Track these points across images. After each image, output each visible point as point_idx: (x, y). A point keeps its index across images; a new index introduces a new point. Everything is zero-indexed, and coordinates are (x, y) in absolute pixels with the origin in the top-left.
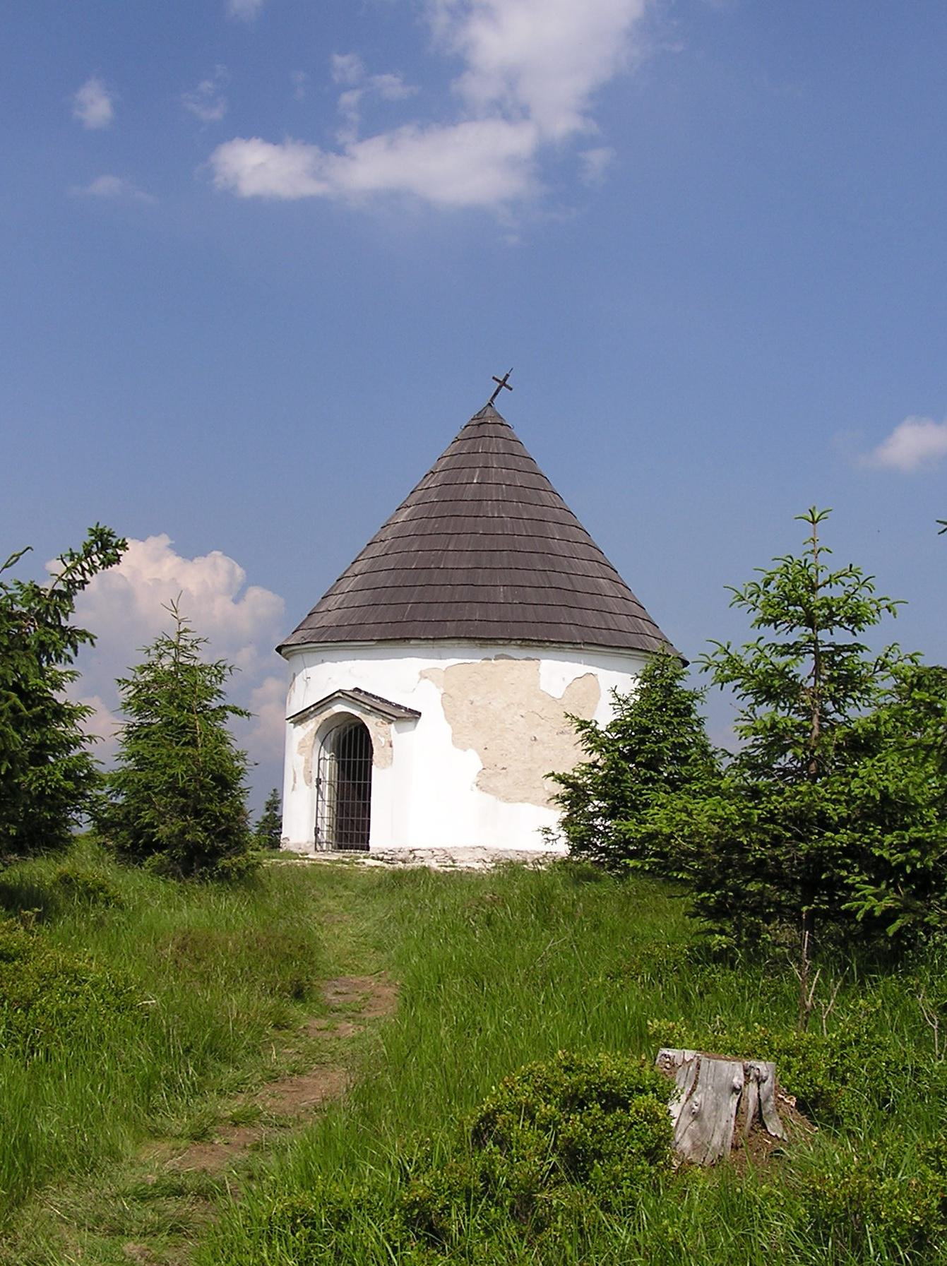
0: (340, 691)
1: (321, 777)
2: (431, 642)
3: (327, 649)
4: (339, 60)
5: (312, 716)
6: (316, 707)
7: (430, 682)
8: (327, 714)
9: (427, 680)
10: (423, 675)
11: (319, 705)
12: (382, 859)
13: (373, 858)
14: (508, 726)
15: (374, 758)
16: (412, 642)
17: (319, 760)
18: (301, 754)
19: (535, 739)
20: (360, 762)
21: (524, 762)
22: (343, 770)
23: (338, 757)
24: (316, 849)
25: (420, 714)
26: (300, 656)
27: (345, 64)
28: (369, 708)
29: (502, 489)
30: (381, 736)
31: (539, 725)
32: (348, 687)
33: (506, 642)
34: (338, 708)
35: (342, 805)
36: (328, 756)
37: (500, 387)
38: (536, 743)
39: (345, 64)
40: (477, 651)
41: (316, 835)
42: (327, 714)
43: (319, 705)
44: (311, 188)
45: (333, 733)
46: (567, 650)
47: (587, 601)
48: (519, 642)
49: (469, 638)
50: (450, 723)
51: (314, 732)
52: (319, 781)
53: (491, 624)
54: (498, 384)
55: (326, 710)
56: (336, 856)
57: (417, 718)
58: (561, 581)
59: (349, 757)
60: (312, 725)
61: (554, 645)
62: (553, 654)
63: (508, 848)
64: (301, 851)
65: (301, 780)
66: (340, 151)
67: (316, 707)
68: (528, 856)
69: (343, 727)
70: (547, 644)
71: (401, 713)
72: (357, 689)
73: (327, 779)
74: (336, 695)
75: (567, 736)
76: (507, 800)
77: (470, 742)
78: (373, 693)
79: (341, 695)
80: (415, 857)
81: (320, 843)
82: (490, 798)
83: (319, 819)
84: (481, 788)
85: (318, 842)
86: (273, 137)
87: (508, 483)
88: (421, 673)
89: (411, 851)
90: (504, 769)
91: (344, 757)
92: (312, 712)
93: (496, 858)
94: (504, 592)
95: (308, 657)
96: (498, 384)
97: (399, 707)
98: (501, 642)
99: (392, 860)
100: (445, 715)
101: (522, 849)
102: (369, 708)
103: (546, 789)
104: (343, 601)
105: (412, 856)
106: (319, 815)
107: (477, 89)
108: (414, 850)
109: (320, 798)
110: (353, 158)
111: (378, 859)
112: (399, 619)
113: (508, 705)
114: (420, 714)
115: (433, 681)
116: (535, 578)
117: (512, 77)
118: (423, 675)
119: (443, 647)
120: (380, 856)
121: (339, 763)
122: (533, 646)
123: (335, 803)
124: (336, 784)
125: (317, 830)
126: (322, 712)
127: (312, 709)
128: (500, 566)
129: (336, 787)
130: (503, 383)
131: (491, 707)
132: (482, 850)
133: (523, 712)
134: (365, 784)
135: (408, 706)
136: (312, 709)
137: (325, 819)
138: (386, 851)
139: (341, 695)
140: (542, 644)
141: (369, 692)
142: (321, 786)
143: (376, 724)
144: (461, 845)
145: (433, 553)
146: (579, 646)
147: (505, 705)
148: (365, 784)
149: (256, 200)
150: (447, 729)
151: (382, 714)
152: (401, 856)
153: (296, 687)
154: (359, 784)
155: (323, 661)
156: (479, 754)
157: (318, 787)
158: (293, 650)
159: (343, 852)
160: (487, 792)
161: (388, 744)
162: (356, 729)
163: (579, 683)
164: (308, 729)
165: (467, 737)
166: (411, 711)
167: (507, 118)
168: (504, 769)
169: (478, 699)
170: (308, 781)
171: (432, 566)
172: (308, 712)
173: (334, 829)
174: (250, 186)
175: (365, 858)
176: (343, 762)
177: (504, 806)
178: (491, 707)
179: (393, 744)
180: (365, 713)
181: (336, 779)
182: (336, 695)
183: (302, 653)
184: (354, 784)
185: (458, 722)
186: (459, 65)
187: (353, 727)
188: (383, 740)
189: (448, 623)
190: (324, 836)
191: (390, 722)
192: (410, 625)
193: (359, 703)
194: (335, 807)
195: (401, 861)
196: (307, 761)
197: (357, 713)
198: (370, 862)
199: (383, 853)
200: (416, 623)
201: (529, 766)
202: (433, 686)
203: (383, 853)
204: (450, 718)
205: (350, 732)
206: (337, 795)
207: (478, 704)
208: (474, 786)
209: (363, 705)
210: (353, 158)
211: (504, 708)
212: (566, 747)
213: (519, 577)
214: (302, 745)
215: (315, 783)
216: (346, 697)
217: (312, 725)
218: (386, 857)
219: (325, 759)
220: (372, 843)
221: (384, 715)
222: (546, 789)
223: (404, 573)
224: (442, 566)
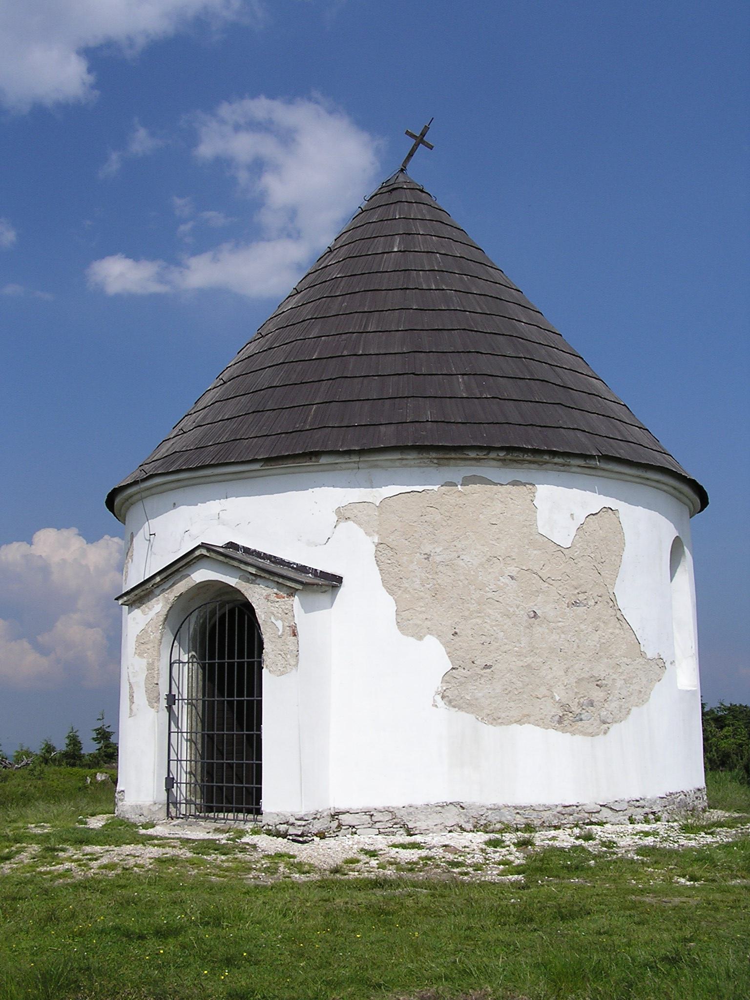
0: (203, 546)
1: (175, 691)
2: (355, 459)
3: (180, 485)
4: (178, 202)
5: (157, 591)
6: (163, 575)
7: (355, 526)
8: (182, 587)
9: (350, 523)
10: (343, 515)
11: (169, 572)
12: (284, 835)
13: (269, 833)
14: (490, 595)
15: (264, 656)
16: (324, 460)
17: (171, 665)
18: (140, 655)
19: (535, 615)
20: (241, 665)
21: (519, 655)
22: (211, 679)
23: (202, 657)
24: (168, 812)
25: (340, 580)
26: (140, 505)
27: (181, 205)
28: (253, 571)
29: (436, 258)
30: (277, 619)
31: (539, 591)
32: (218, 540)
33: (481, 455)
34: (201, 575)
35: (211, 738)
36: (185, 658)
37: (416, 146)
38: (536, 621)
39: (181, 205)
40: (432, 471)
41: (168, 790)
42: (182, 587)
43: (169, 572)
44: (156, 288)
45: (193, 618)
46: (574, 469)
47: (587, 403)
48: (502, 454)
49: (420, 449)
50: (391, 592)
51: (162, 618)
52: (171, 700)
53: (454, 426)
54: (414, 141)
55: (180, 580)
56: (200, 832)
57: (334, 587)
58: (543, 372)
59: (221, 657)
60: (158, 606)
61: (556, 460)
62: (552, 475)
63: (500, 801)
64: (142, 819)
65: (141, 697)
66: (179, 264)
67: (163, 575)
68: (535, 814)
69: (209, 608)
70: (546, 457)
71: (309, 578)
72: (231, 545)
73: (185, 696)
74: (197, 553)
75: (581, 610)
76: (495, 720)
77: (428, 623)
78: (259, 549)
79: (204, 552)
80: (340, 826)
81: (175, 804)
82: (466, 719)
83: (173, 764)
84: (450, 702)
85: (171, 801)
86: (134, 254)
87: (443, 252)
88: (338, 511)
89: (332, 816)
90: (487, 667)
91: (212, 657)
92: (158, 585)
93: (483, 822)
94: (464, 383)
95: (151, 503)
96: (414, 141)
97: (303, 569)
98: (472, 455)
99: (302, 835)
100: (383, 580)
101: (523, 805)
102: (253, 571)
103: (557, 698)
104: (206, 415)
105: (335, 824)
106: (173, 756)
107: (269, 219)
108: (338, 814)
109: (174, 729)
110: (188, 268)
111: (278, 834)
112: (298, 426)
113: (488, 560)
114: (340, 580)
115: (360, 525)
116: (510, 367)
117: (292, 213)
118: (343, 515)
119: (376, 466)
120: (282, 828)
121: (204, 668)
122: (523, 461)
123: (199, 735)
124: (200, 702)
125: (170, 782)
126: (174, 584)
127: (158, 579)
128: (452, 349)
129: (200, 708)
130: (420, 140)
131: (462, 563)
132: (455, 810)
133: (513, 570)
134: (250, 703)
135: (320, 568)
136: (158, 579)
137: (184, 763)
138: (292, 820)
139: (204, 552)
140: (538, 458)
141: (252, 548)
142: (175, 707)
143: (267, 598)
144: (419, 802)
145: (344, 337)
146: (592, 463)
147: (484, 560)
148: (250, 703)
149: (118, 297)
150: (387, 605)
151: (276, 579)
152: (317, 826)
153: (134, 553)
154: (240, 703)
155: (175, 506)
156: (446, 645)
157: (169, 708)
158: (131, 497)
159: (216, 820)
160: (460, 708)
161: (288, 631)
162: (232, 612)
163: (594, 522)
164: (152, 614)
165: (424, 616)
166: (324, 575)
167: (289, 236)
168: (487, 667)
169: (438, 550)
170: (153, 700)
171: (345, 353)
172: (150, 585)
173: (199, 778)
174: (114, 287)
175: (255, 832)
176: (212, 666)
177: (490, 732)
178: (462, 563)
179: (299, 629)
180: (248, 581)
181: (200, 696)
182: (197, 553)
183: (142, 499)
184: (230, 703)
185: (406, 591)
186: (259, 202)
187: (227, 608)
188: (279, 624)
189: (382, 428)
190: (182, 792)
191: (292, 592)
192: (318, 434)
193: (236, 564)
194: (199, 741)
195: (316, 835)
196: (151, 667)
197: (232, 581)
198: (267, 844)
199: (287, 823)
200: (327, 430)
201: (529, 660)
202: (361, 532)
203: (287, 823)
204: (392, 583)
205: (222, 618)
206: (203, 722)
207: (438, 559)
208: (438, 698)
209: (242, 566)
210: (188, 268)
211: (482, 565)
212: (583, 627)
213: (484, 364)
214: (141, 641)
215: (164, 703)
216: (214, 555)
217: (158, 606)
218: (292, 831)
219: (180, 662)
220: (266, 804)
221: (281, 580)
222: (557, 698)
223: (300, 366)
224: (361, 352)
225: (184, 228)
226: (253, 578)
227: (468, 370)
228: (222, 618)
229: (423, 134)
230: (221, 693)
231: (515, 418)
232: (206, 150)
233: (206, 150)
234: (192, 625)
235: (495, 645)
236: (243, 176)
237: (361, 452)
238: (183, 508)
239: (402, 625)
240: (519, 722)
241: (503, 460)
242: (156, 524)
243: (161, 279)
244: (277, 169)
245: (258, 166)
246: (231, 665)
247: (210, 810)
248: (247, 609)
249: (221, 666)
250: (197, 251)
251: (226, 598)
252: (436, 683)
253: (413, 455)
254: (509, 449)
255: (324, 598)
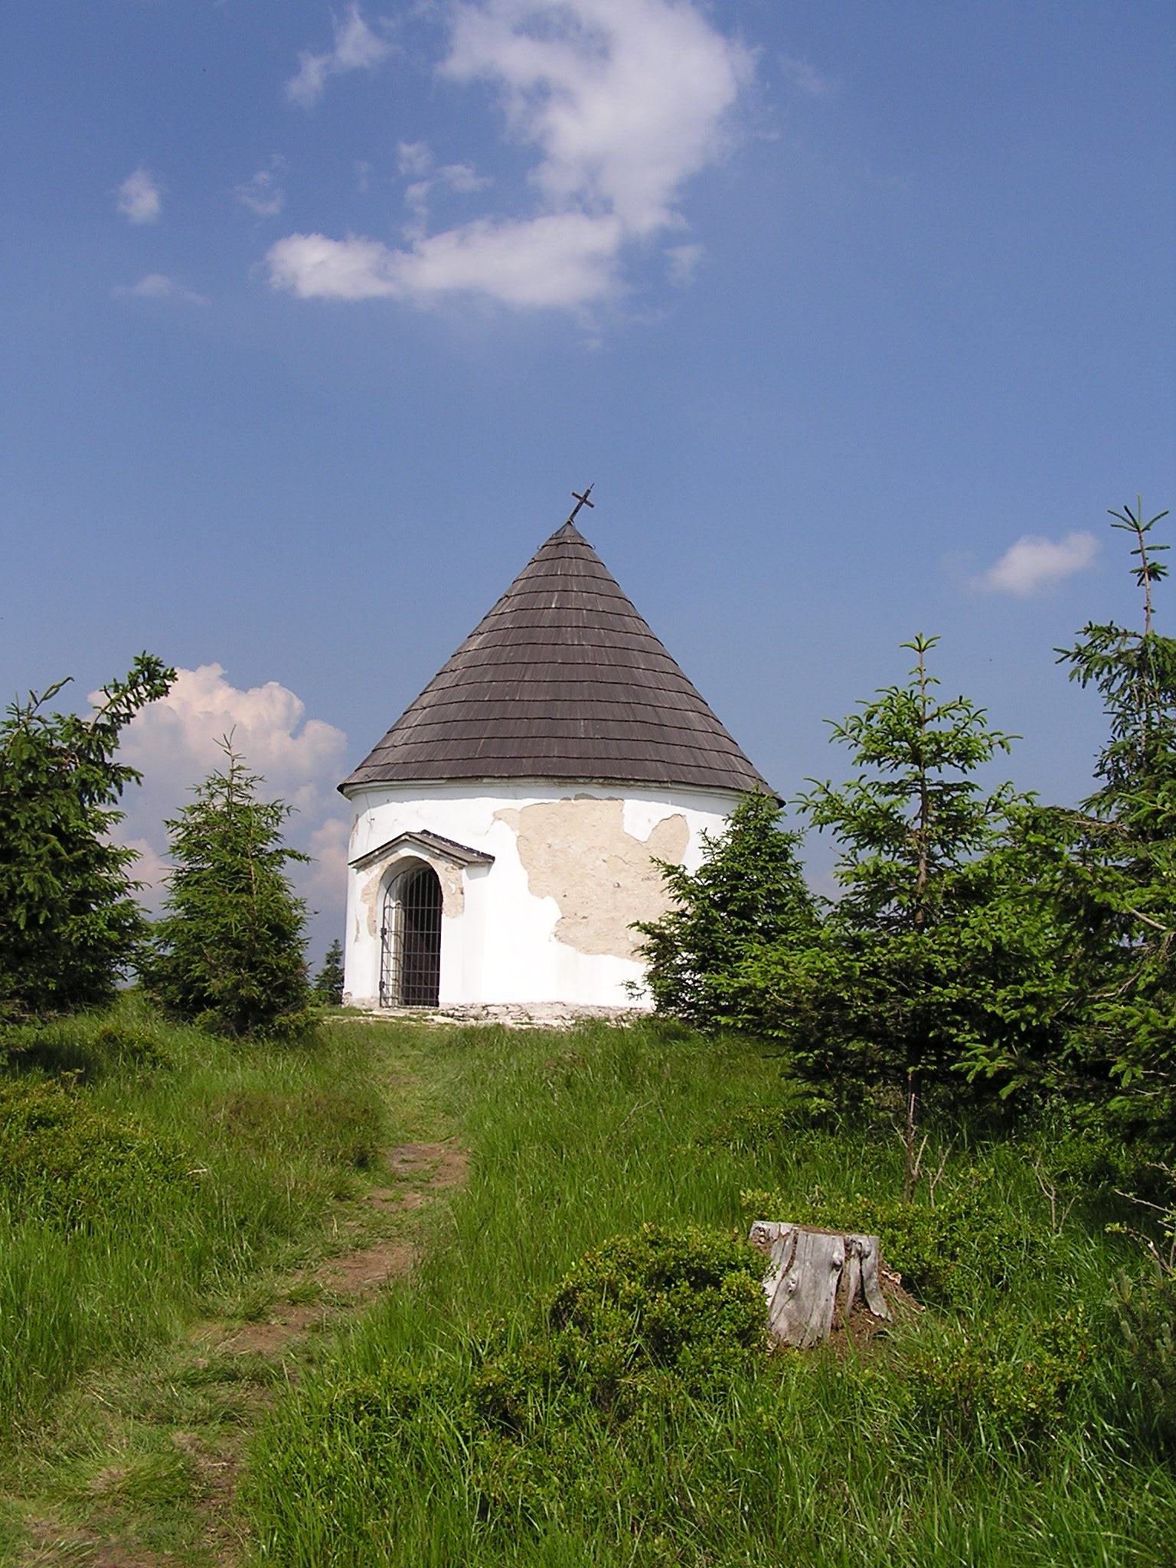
1: (386, 926)
3: (392, 788)
4: (406, 150)
8: (393, 859)
10: (497, 817)
12: (452, 1016)
13: (443, 1015)
16: (485, 780)
19: (619, 886)
22: (410, 919)
23: (405, 905)
25: (493, 858)
26: (364, 796)
27: (412, 154)
32: (416, 829)
33: (587, 781)
34: (405, 852)
35: (409, 957)
36: (393, 904)
37: (581, 504)
39: (412, 154)
40: (556, 790)
41: (381, 990)
42: (393, 859)
45: (399, 879)
47: (674, 736)
48: (601, 781)
49: (547, 776)
50: (526, 868)
52: (384, 931)
56: (402, 1013)
59: (417, 905)
60: (377, 870)
62: (638, 793)
64: (364, 1007)
65: (364, 930)
66: (407, 248)
69: (409, 873)
70: (632, 782)
71: (473, 857)
72: (425, 832)
73: (393, 929)
80: (488, 1014)
81: (385, 998)
82: (569, 950)
83: (384, 973)
85: (383, 997)
86: (334, 233)
88: (494, 814)
91: (411, 905)
92: (377, 857)
95: (372, 797)
97: (471, 850)
98: (581, 781)
107: (555, 180)
109: (385, 950)
110: (421, 256)
111: (448, 1016)
112: (471, 755)
114: (493, 858)
116: (619, 712)
117: (593, 168)
118: (497, 817)
120: (451, 1012)
125: (382, 984)
130: (584, 500)
132: (560, 1006)
134: (434, 935)
135: (481, 850)
140: (626, 783)
143: (446, 869)
144: (537, 1000)
146: (666, 785)
148: (434, 935)
150: (523, 876)
152: (473, 1012)
154: (428, 935)
155: (388, 801)
157: (383, 937)
161: (459, 891)
162: (424, 875)
164: (373, 875)
166: (484, 855)
167: (588, 212)
175: (434, 1014)
176: (411, 911)
179: (465, 891)
184: (422, 935)
186: (536, 155)
188: (453, 886)
190: (390, 991)
191: (462, 867)
192: (483, 762)
196: (371, 910)
197: (425, 857)
198: (440, 1019)
201: (612, 914)
202: (507, 828)
204: (527, 862)
210: (421, 256)
211: (584, 852)
214: (365, 893)
215: (379, 934)
217: (377, 870)
218: (456, 1014)
223: (477, 705)
225: (416, 191)
226: (438, 857)
227: (588, 716)
228: (418, 879)
229: (586, 496)
230: (416, 929)
231: (614, 754)
232: (458, 66)
233: (458, 66)
234: (398, 882)
235: (590, 904)
236: (516, 108)
237: (508, 777)
238: (393, 804)
239: (532, 889)
240: (604, 953)
241: (602, 784)
242: (374, 812)
243: (381, 273)
244: (569, 98)
245: (541, 93)
246: (423, 911)
247: (407, 1003)
248: (432, 875)
249: (417, 911)
250: (435, 228)
251: (419, 866)
252: (551, 926)
253: (543, 780)
254: (605, 778)
255: (483, 870)
